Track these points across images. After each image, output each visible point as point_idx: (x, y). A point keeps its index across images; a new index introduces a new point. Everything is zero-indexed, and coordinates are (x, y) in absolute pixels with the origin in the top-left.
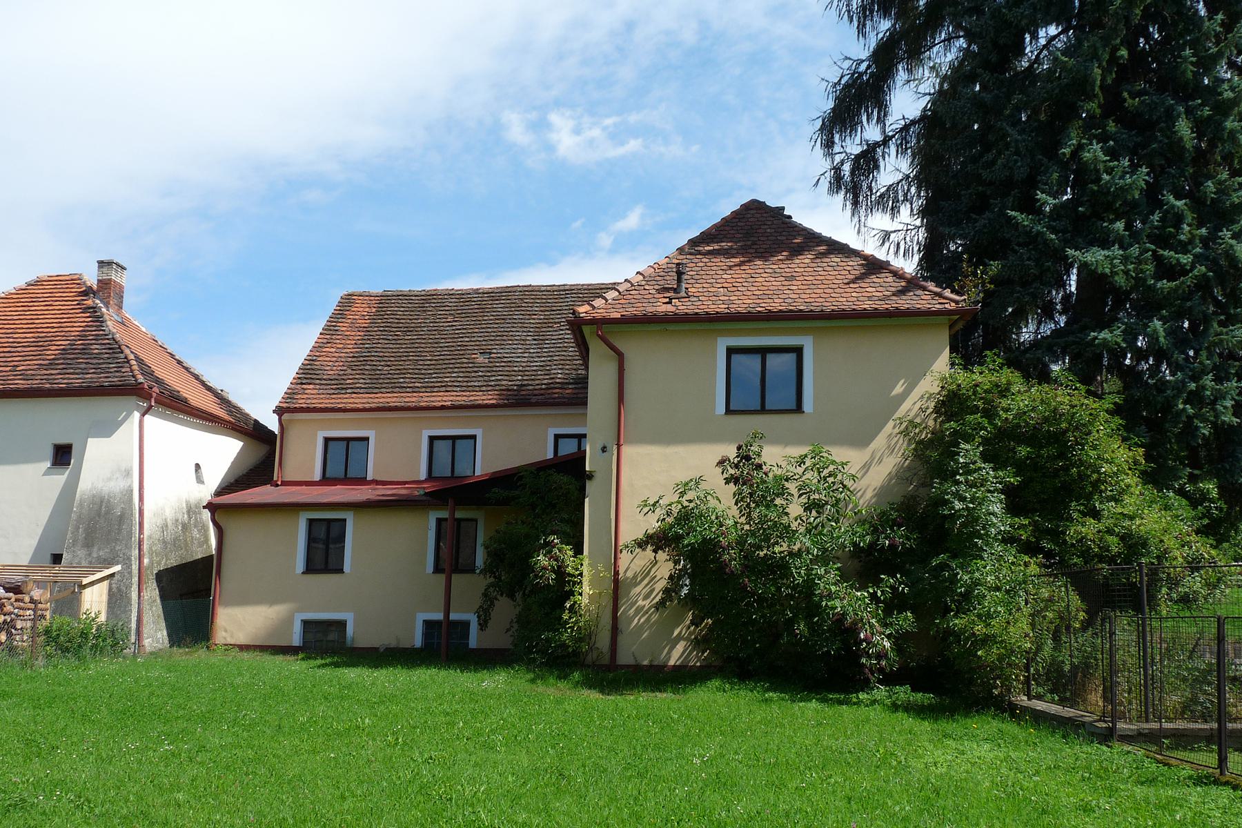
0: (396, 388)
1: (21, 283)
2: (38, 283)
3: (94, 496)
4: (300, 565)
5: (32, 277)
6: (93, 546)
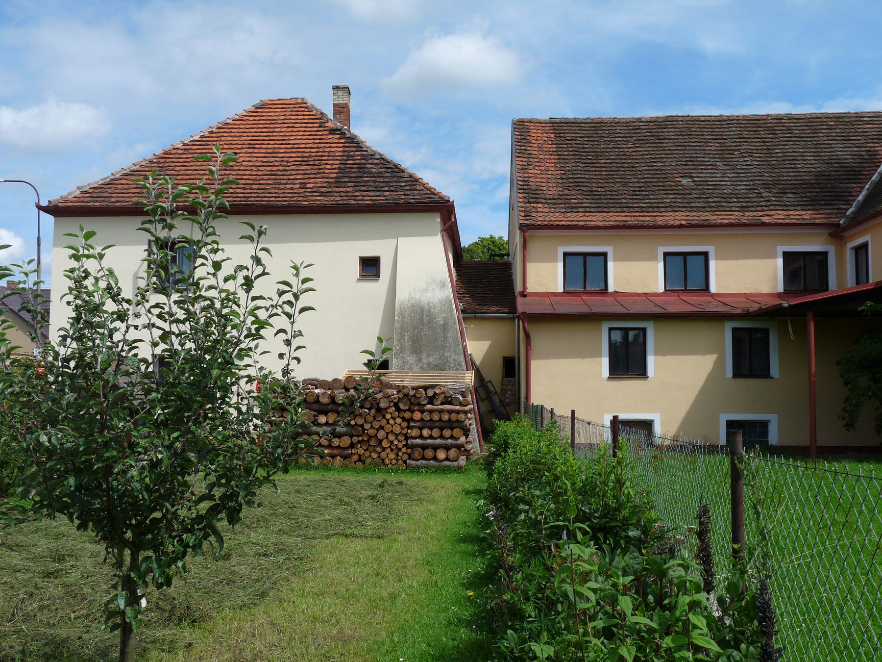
0: (622, 208)
1: (249, 107)
2: (263, 106)
3: (413, 306)
4: (606, 372)
5: (256, 101)
6: (421, 352)
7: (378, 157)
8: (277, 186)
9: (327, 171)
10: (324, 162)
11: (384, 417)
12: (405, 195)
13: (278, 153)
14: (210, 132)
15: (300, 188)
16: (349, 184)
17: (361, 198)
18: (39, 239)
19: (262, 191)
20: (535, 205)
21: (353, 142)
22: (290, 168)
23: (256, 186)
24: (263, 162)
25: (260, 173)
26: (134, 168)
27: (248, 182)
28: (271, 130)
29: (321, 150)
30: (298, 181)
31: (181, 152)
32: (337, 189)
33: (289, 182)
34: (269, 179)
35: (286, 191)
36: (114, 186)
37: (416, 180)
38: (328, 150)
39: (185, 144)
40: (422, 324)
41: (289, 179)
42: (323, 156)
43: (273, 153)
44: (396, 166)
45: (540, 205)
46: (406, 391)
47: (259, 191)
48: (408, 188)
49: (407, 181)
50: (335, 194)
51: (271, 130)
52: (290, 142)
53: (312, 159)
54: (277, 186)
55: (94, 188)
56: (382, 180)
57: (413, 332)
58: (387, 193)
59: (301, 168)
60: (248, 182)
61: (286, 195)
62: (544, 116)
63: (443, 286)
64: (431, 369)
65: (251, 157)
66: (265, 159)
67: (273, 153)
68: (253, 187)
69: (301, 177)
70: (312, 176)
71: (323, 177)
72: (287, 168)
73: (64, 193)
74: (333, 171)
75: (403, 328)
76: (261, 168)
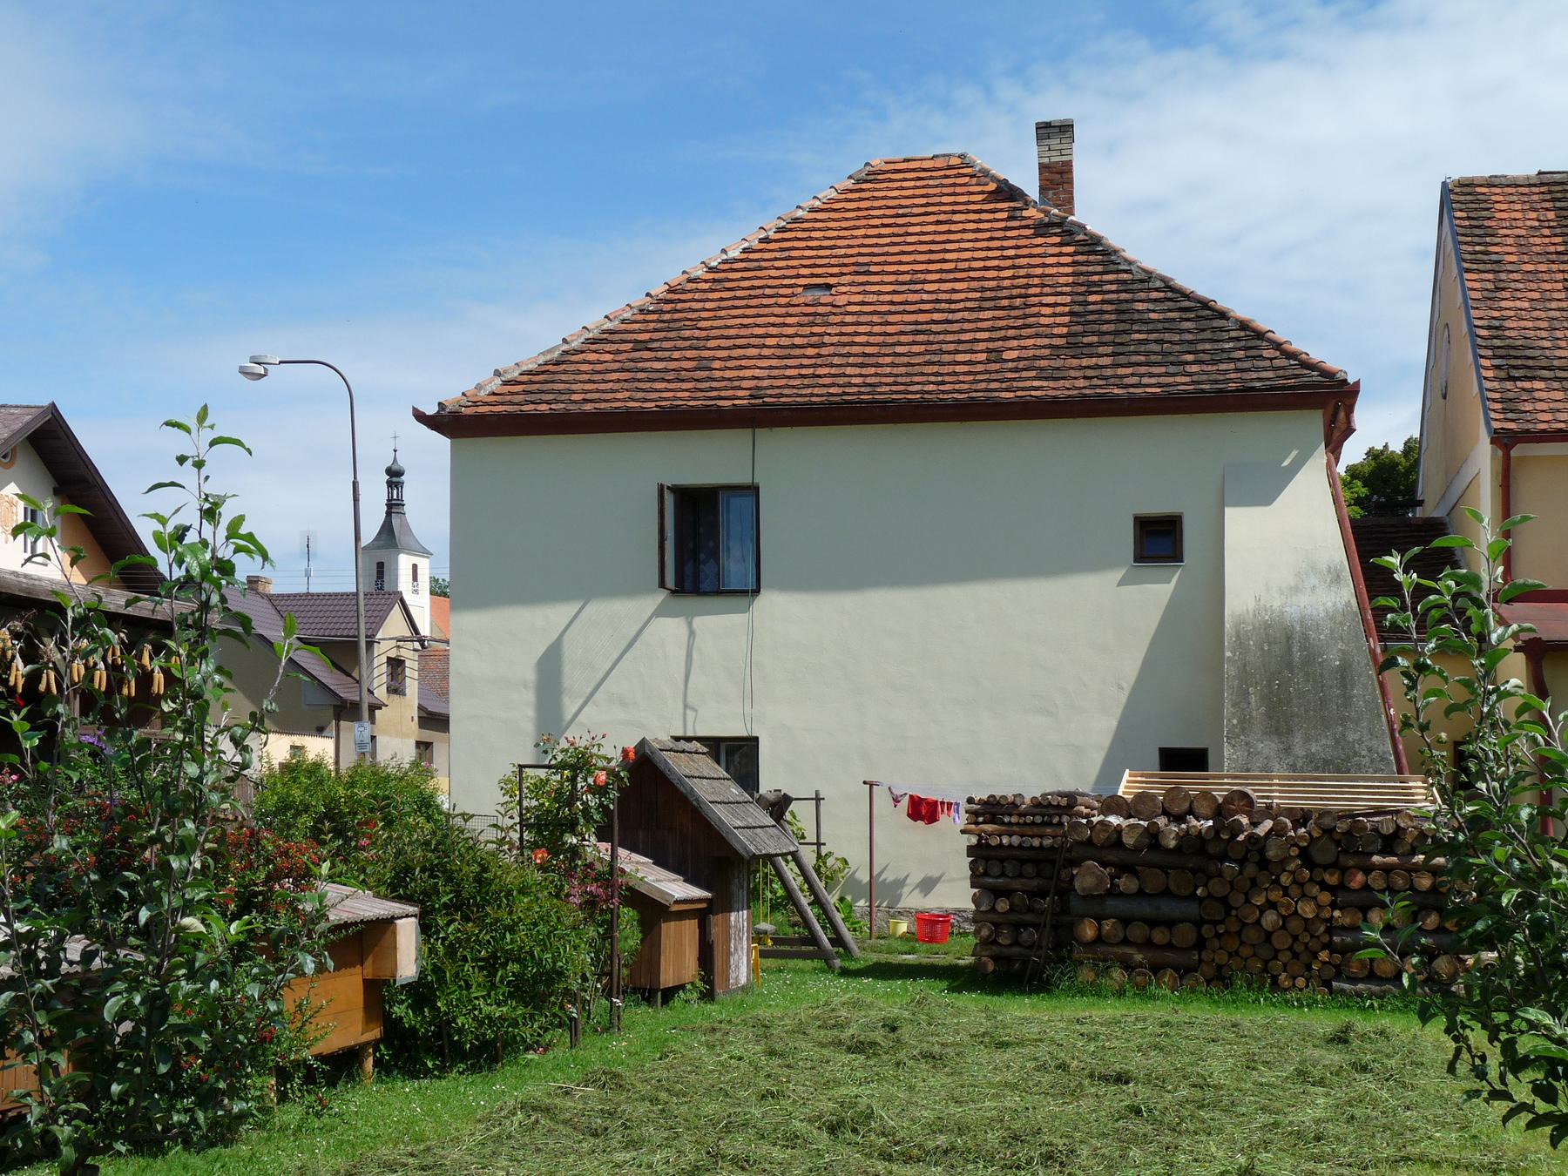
3: (1267, 626)
6: (1290, 732)
7: (1158, 284)
8: (935, 358)
9: (1043, 321)
10: (1036, 300)
11: (1277, 881)
12: (1237, 370)
13: (925, 282)
14: (761, 241)
15: (989, 361)
16: (1101, 350)
17: (1134, 380)
18: (355, 484)
19: (902, 370)
20: (1527, 385)
21: (1095, 253)
22: (959, 315)
23: (888, 360)
24: (892, 303)
25: (890, 329)
26: (608, 325)
27: (868, 350)
28: (901, 230)
29: (1022, 272)
30: (982, 346)
31: (706, 286)
32: (1075, 362)
33: (961, 347)
34: (914, 343)
35: (958, 369)
36: (572, 368)
37: (1260, 335)
38: (1039, 271)
39: (711, 270)
40: (1290, 666)
41: (960, 342)
42: (1028, 286)
43: (911, 282)
44: (1205, 304)
45: (1538, 385)
46: (1327, 821)
47: (895, 370)
48: (1241, 354)
49: (1238, 339)
50: (1073, 373)
51: (901, 230)
52: (948, 256)
53: (1005, 293)
54: (935, 358)
55: (529, 373)
56: (1177, 338)
57: (1269, 686)
58: (1195, 368)
59: (983, 315)
60: (868, 350)
61: (961, 377)
62: (1523, 167)
63: (1337, 579)
64: (1317, 769)
65: (866, 293)
66: (897, 298)
67: (911, 282)
68: (881, 360)
69: (986, 335)
70: (1011, 333)
71: (1037, 336)
72: (950, 316)
73: (469, 386)
74: (1058, 320)
75: (1244, 675)
76: (891, 318)
